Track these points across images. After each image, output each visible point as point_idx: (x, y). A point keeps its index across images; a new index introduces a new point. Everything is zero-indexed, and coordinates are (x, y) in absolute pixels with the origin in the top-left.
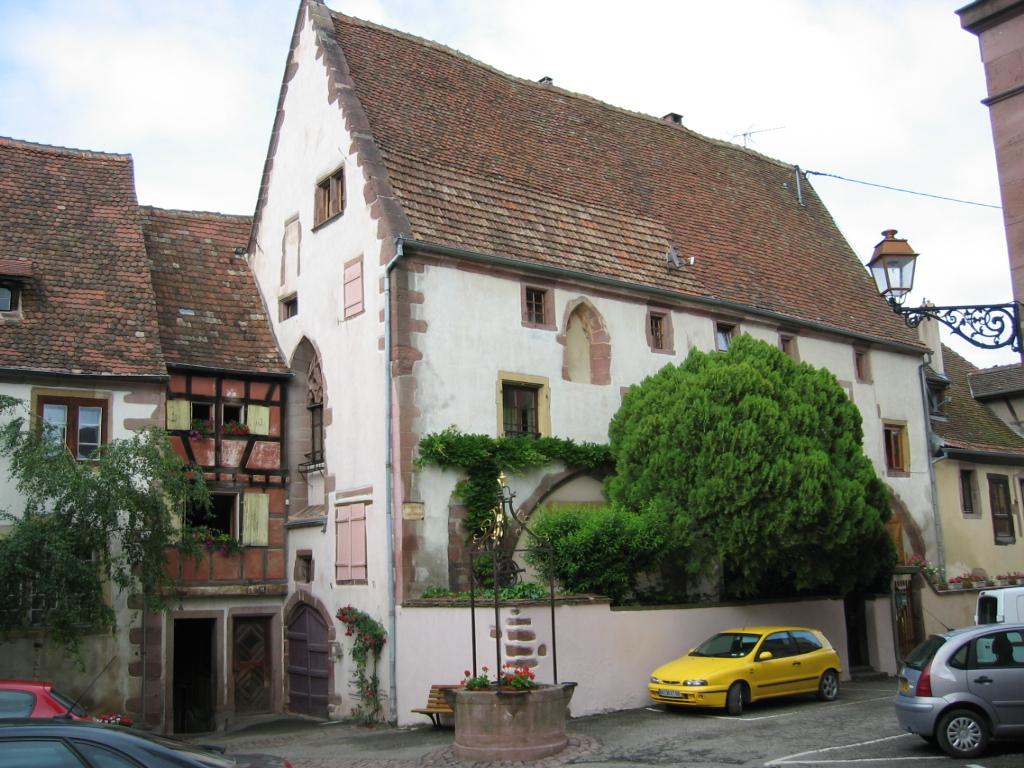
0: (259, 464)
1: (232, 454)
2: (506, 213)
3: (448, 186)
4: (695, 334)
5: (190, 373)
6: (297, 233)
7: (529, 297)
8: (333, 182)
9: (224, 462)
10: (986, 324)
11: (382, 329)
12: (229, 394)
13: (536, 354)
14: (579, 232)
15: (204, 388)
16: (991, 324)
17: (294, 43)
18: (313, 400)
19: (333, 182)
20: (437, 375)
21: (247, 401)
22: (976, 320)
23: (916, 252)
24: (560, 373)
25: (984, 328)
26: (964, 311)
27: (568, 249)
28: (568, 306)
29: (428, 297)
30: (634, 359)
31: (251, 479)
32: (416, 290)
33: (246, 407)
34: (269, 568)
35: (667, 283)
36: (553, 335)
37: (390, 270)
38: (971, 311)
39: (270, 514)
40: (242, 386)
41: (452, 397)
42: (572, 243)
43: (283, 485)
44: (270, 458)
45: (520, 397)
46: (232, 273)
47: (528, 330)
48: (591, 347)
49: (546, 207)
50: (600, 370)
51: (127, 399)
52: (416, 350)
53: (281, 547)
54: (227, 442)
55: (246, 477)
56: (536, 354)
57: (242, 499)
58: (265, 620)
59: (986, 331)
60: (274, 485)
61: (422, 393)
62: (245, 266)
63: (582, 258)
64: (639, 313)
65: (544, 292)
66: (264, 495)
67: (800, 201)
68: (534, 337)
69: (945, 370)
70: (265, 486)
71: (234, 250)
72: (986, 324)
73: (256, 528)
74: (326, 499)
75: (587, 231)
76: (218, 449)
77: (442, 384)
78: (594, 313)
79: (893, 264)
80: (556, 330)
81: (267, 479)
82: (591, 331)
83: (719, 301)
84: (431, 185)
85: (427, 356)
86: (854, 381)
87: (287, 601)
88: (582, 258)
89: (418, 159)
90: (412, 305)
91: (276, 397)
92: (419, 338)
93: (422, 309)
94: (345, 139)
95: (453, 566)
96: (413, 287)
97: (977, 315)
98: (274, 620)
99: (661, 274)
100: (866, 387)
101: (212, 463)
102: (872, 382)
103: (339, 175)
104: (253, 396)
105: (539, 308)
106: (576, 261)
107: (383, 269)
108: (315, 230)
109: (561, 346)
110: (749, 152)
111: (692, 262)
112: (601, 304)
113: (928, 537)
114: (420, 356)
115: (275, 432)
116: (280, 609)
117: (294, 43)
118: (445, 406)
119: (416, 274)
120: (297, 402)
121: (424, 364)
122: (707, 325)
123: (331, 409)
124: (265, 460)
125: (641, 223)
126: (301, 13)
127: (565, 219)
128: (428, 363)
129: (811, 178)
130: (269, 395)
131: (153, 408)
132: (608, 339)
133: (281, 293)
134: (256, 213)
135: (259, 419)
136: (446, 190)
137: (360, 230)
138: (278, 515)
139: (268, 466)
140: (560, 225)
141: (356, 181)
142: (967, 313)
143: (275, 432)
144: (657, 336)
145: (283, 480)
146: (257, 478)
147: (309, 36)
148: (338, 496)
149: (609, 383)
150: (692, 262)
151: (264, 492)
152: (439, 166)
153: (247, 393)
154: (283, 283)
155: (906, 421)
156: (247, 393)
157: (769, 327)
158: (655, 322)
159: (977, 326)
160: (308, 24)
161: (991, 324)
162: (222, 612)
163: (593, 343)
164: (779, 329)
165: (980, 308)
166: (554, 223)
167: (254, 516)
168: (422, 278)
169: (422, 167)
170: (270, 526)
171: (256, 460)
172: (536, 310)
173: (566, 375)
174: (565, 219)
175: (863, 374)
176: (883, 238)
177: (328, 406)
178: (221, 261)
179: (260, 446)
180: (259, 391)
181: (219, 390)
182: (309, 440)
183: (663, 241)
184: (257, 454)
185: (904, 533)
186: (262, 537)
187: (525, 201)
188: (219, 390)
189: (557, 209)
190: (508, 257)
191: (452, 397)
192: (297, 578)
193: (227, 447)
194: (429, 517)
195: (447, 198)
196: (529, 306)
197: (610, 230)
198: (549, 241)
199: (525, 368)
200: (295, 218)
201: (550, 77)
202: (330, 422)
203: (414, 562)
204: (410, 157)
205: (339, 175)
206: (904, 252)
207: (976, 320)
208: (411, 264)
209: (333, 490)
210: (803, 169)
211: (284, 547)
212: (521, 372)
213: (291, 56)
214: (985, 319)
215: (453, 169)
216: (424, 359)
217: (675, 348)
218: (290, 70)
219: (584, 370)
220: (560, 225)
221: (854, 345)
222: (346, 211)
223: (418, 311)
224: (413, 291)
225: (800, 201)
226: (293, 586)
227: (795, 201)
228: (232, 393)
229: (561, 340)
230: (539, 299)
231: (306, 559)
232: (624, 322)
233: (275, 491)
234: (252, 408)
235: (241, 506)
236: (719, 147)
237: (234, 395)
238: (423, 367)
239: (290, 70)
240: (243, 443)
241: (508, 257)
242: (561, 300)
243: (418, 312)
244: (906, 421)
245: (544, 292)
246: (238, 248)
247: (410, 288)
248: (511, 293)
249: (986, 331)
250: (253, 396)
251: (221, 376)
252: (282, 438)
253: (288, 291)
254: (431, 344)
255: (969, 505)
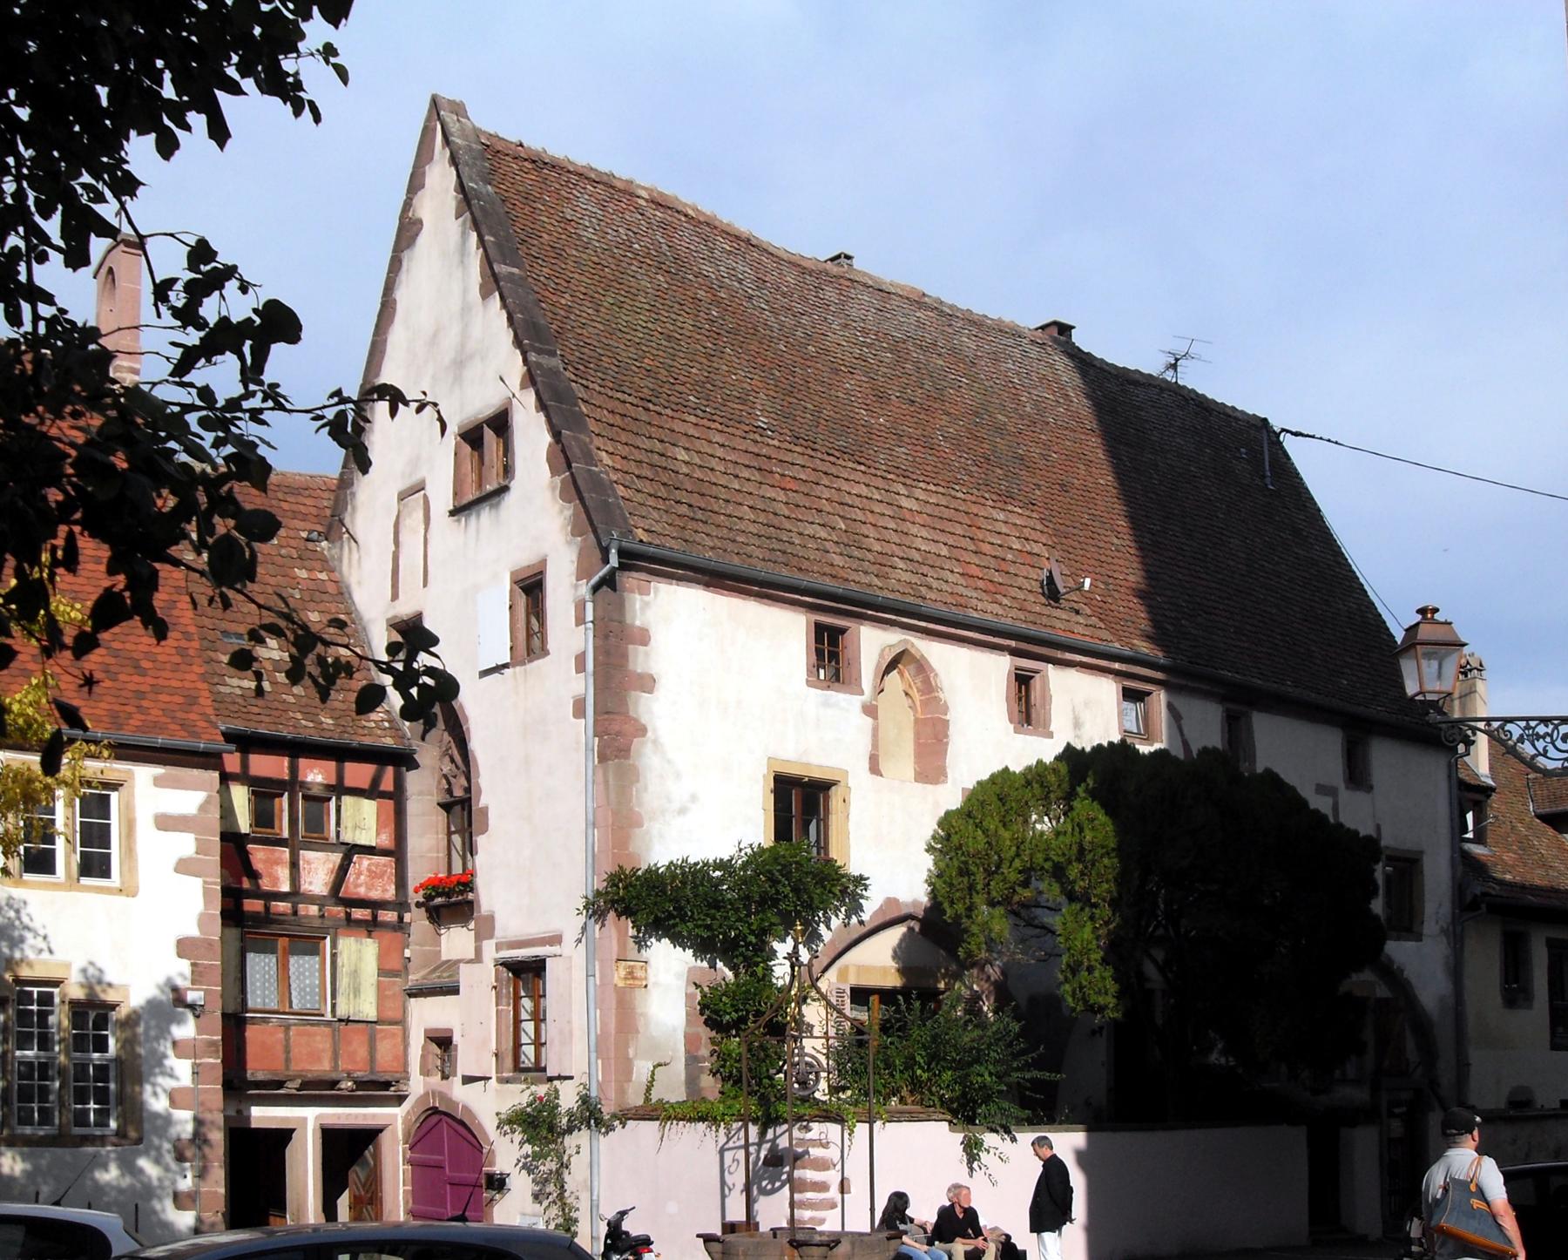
0: (362, 892)
1: (318, 871)
2: (782, 496)
3: (686, 449)
4: (1086, 704)
5: (247, 743)
6: (420, 514)
7: (819, 639)
8: (489, 435)
9: (305, 887)
10: (1553, 743)
11: (582, 685)
12: (310, 778)
13: (831, 733)
14: (904, 524)
15: (267, 765)
16: (1559, 743)
17: (416, 184)
18: (450, 791)
19: (489, 435)
20: (669, 762)
21: (339, 789)
22: (1539, 737)
23: (1464, 640)
24: (865, 764)
25: (1550, 748)
26: (1523, 724)
27: (880, 559)
28: (881, 655)
29: (659, 637)
30: (988, 739)
31: (348, 915)
32: (638, 623)
33: (339, 799)
34: (379, 1056)
35: (1045, 620)
36: (855, 702)
37: (595, 589)
38: (1533, 724)
39: (382, 972)
40: (332, 765)
41: (694, 798)
42: (887, 549)
43: (400, 926)
44: (379, 882)
45: (801, 800)
46: (303, 574)
47: (816, 694)
48: (917, 721)
49: (845, 486)
50: (931, 759)
51: (158, 782)
52: (636, 720)
53: (396, 1023)
54: (306, 855)
55: (339, 911)
56: (831, 733)
57: (334, 945)
58: (369, 1136)
59: (1552, 752)
60: (385, 925)
61: (646, 789)
62: (326, 564)
63: (906, 577)
64: (999, 667)
65: (843, 631)
66: (369, 940)
67: (1268, 481)
68: (826, 704)
69: (1491, 768)
70: (371, 927)
71: (304, 535)
72: (1553, 743)
73: (357, 992)
74: (478, 951)
75: (914, 530)
76: (294, 865)
77: (678, 776)
78: (923, 668)
79: (1428, 656)
80: (862, 693)
81: (267, 908)
82: (917, 696)
83: (1127, 652)
84: (658, 446)
85: (655, 730)
86: (1342, 786)
87: (407, 1105)
88: (906, 577)
89: (635, 401)
90: (631, 647)
91: (387, 784)
92: (642, 701)
93: (647, 654)
94: (515, 367)
95: (692, 1060)
96: (634, 618)
97: (1542, 729)
98: (385, 1138)
99: (1037, 604)
100: (1360, 797)
101: (285, 887)
102: (1370, 789)
103: (501, 422)
104: (349, 782)
105: (834, 656)
106: (898, 583)
107: (584, 589)
108: (459, 510)
109: (869, 720)
110: (1185, 393)
111: (1087, 585)
112: (937, 653)
113: (1444, 1036)
114: (643, 731)
115: (386, 840)
116: (394, 1120)
117: (416, 184)
118: (682, 811)
119: (638, 596)
120: (420, 793)
121: (650, 745)
122: (1106, 690)
123: (487, 808)
124: (369, 889)
125: (1001, 516)
126: (427, 132)
127: (878, 508)
128: (655, 742)
129: (1288, 442)
130: (376, 781)
131: (198, 797)
132: (946, 709)
133: (390, 615)
134: (342, 474)
135: (361, 820)
136: (682, 455)
137: (536, 517)
138: (394, 973)
139: (375, 894)
140: (871, 518)
141: (532, 436)
142: (1528, 727)
143: (386, 840)
144: (1026, 705)
145: (401, 918)
146: (359, 914)
147: (441, 177)
148: (499, 947)
149: (945, 782)
150: (1087, 585)
151: (369, 936)
152: (669, 412)
153: (340, 776)
154: (395, 596)
155: (1421, 852)
156: (340, 776)
157: (1207, 695)
158: (1022, 681)
159: (1540, 744)
160: (440, 153)
161: (1559, 743)
162: (305, 1119)
163: (920, 716)
164: (1222, 699)
165: (1545, 721)
166: (860, 515)
167: (355, 974)
168: (646, 605)
169: (644, 416)
170: (380, 988)
171: (357, 886)
172: (829, 655)
173: (875, 769)
174: (878, 508)
175: (1357, 776)
176: (1419, 617)
177: (482, 803)
178: (283, 551)
179: (363, 863)
180: (358, 773)
181: (294, 770)
182: (443, 855)
183: (1036, 548)
184: (359, 874)
185: (1408, 1034)
186: (369, 1010)
187: (813, 477)
188: (294, 770)
189: (864, 491)
190: (785, 572)
191: (694, 798)
192: (425, 1072)
193: (309, 863)
194: (655, 984)
195: (685, 470)
196: (819, 653)
197: (949, 527)
198: (852, 542)
199: (810, 759)
200: (419, 488)
201: (849, 253)
202: (484, 830)
203: (631, 1052)
204: (619, 395)
205: (501, 422)
206: (1448, 638)
207: (1539, 737)
208: (630, 580)
209: (491, 936)
210: (1277, 425)
211: (401, 1022)
212: (804, 760)
213: (408, 205)
214: (1551, 736)
215: (693, 419)
216: (649, 734)
217: (1052, 728)
218: (408, 231)
219: (902, 763)
220: (871, 518)
221: (1344, 727)
222: (514, 485)
223: (641, 658)
224: (633, 626)
225: (1268, 481)
226: (417, 1085)
227: (1258, 481)
228: (316, 774)
229: (870, 710)
230: (834, 642)
231: (443, 1042)
232: (972, 679)
233: (388, 936)
234: (347, 800)
235: (334, 956)
236: (1136, 383)
237: (319, 779)
238: (648, 749)
239: (408, 231)
240: (336, 858)
241: (785, 572)
242: (872, 643)
243: (642, 660)
244: (1421, 852)
245: (843, 631)
246: (311, 532)
247: (628, 621)
248: (788, 631)
249: (1552, 752)
250: (348, 783)
251: (297, 749)
252: (397, 852)
253: (404, 609)
254: (662, 713)
255: (1515, 992)
